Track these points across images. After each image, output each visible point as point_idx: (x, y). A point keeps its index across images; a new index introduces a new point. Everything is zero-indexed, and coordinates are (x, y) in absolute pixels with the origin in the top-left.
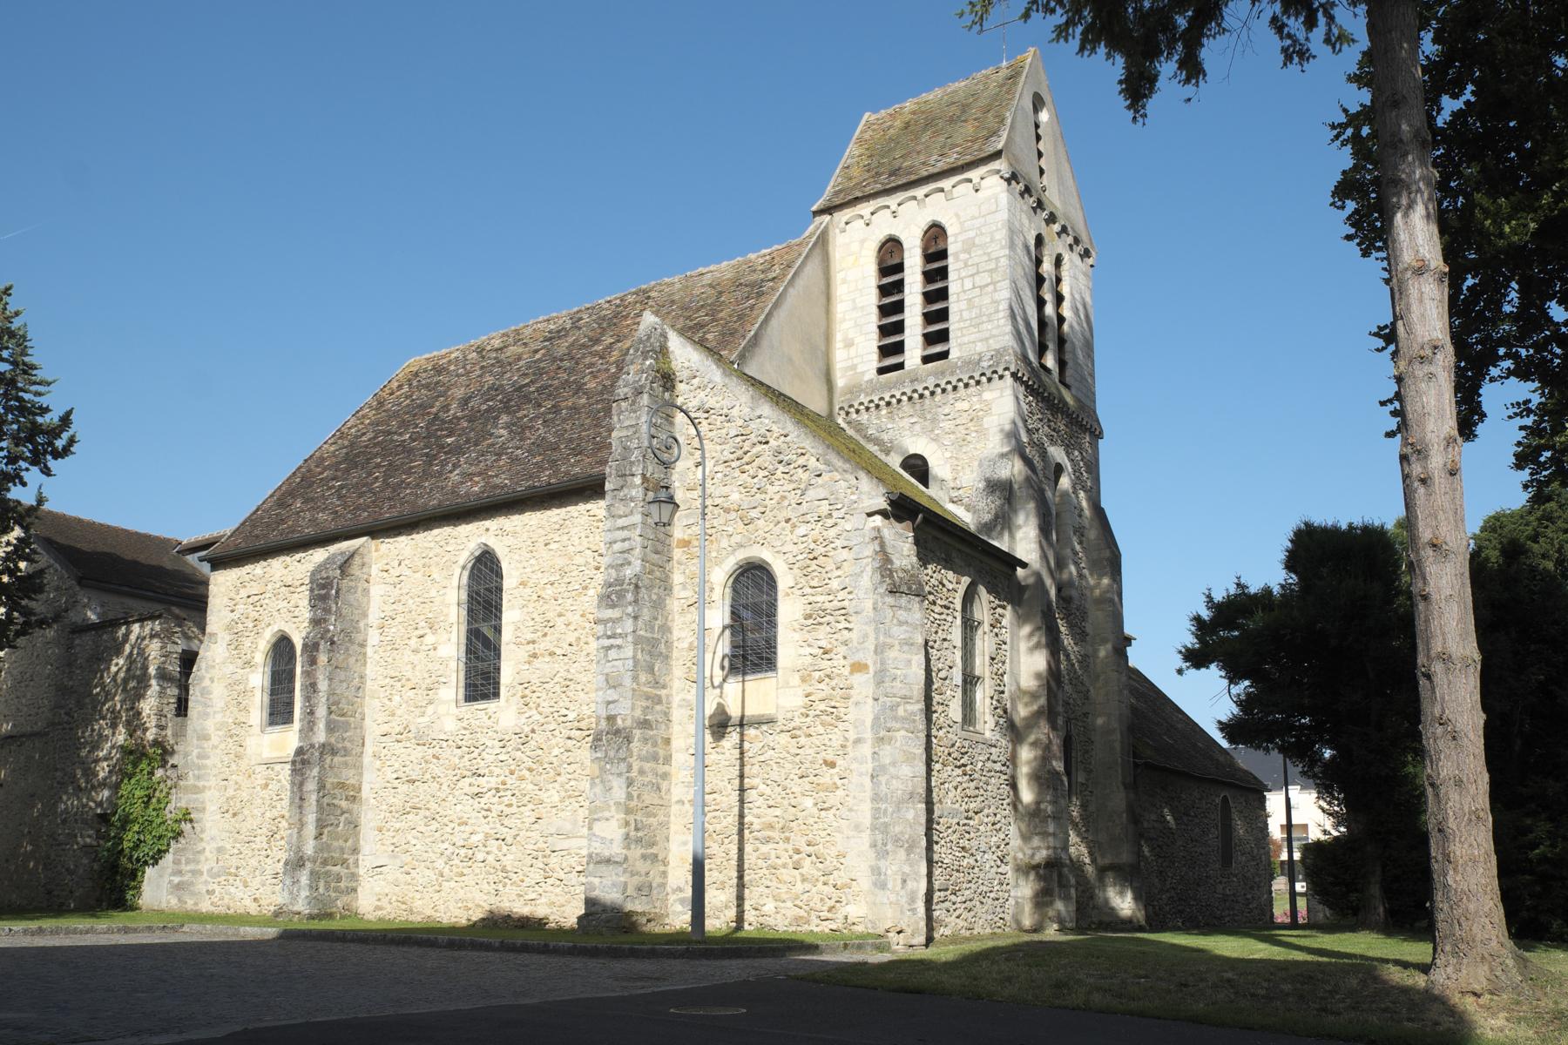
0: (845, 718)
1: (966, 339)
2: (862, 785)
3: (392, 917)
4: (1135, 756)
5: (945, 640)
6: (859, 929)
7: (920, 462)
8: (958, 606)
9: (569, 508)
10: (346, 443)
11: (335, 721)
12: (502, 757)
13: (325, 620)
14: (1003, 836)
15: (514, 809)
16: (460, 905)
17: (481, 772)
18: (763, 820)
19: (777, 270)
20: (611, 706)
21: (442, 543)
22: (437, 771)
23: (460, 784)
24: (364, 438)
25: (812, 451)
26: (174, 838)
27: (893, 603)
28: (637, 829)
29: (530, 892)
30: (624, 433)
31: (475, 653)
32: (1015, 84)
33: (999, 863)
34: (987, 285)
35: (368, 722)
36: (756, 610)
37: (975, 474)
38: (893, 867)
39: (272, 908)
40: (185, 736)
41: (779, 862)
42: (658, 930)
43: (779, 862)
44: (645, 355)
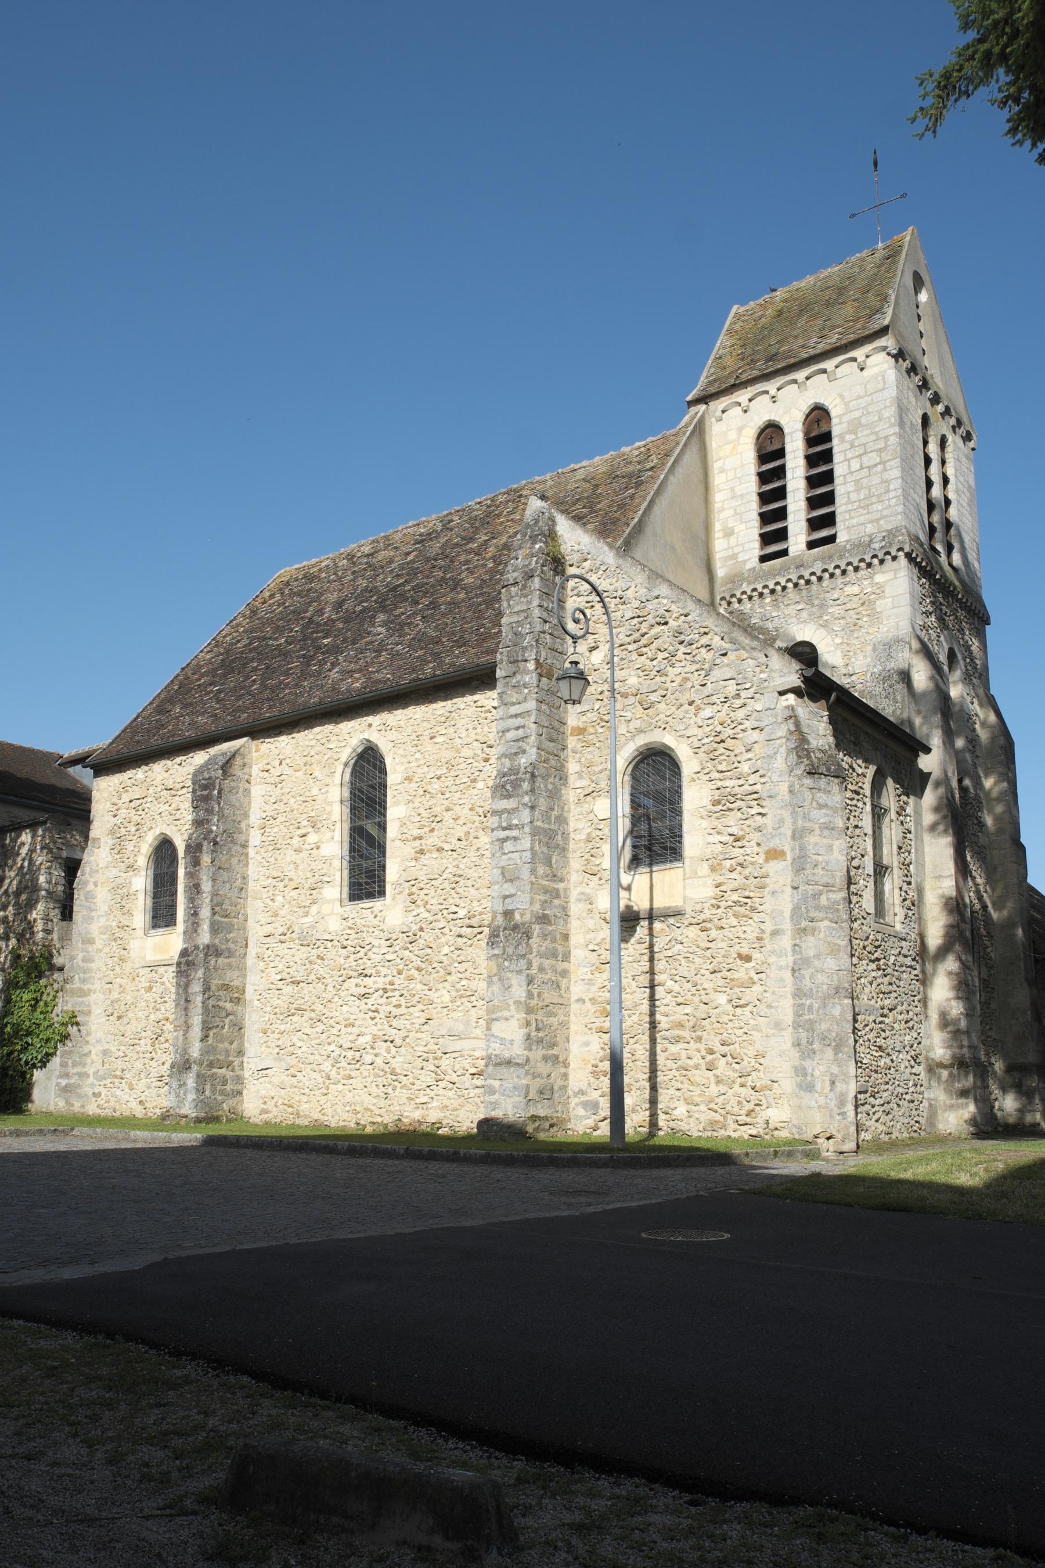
0: (761, 908)
1: (855, 521)
2: (782, 980)
3: (278, 1120)
4: (1035, 951)
5: (856, 827)
6: (784, 1134)
7: (808, 650)
8: (868, 793)
9: (455, 700)
10: (222, 650)
11: (219, 922)
12: (389, 957)
13: (208, 821)
14: (915, 1035)
15: (403, 1010)
16: (348, 1108)
17: (368, 972)
18: (672, 1018)
19: (654, 460)
20: (508, 901)
21: (323, 741)
22: (322, 972)
23: (346, 985)
24: (239, 645)
25: (716, 629)
26: (61, 1041)
27: (812, 785)
28: (538, 1030)
29: (421, 1096)
30: (515, 618)
31: (359, 851)
32: (895, 262)
33: (912, 1063)
34: (876, 465)
35: (250, 922)
36: (659, 797)
37: (869, 659)
38: (821, 1068)
39: (158, 1112)
40: (70, 940)
41: (690, 1062)
42: (559, 1136)
43: (690, 1062)
44: (534, 539)
